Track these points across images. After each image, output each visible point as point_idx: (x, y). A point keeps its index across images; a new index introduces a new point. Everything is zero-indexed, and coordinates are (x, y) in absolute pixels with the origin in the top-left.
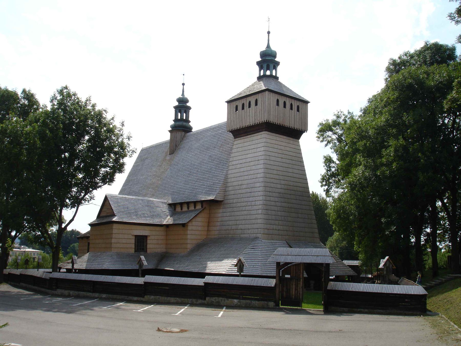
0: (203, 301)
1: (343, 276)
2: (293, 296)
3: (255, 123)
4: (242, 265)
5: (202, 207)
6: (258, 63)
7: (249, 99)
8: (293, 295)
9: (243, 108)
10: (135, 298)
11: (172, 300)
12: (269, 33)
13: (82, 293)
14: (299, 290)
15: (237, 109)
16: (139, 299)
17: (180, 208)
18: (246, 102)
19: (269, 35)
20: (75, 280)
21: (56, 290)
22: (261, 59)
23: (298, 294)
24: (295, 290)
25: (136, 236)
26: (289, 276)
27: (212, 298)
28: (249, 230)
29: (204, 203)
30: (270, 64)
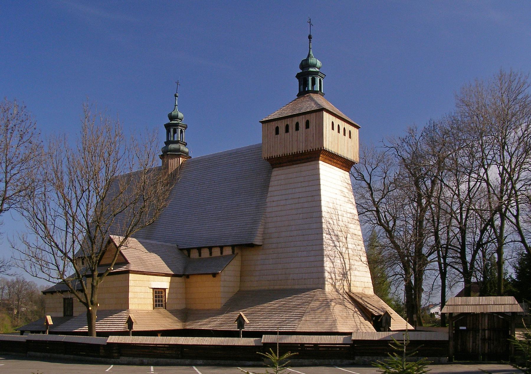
0: (351, 361)
1: (133, 335)
2: (471, 349)
3: (286, 154)
4: (388, 318)
5: (233, 252)
6: (298, 76)
7: (296, 119)
8: (470, 348)
9: (287, 130)
10: (251, 363)
11: (306, 362)
12: (310, 37)
13: (162, 359)
14: (477, 342)
15: (277, 132)
16: (256, 363)
17: (197, 254)
18: (292, 123)
19: (310, 41)
20: (89, 344)
21: (119, 358)
22: (301, 71)
23: (477, 347)
24: (473, 343)
25: (154, 289)
26: (464, 328)
27: (363, 357)
28: (306, 280)
29: (235, 248)
30: (315, 77)
